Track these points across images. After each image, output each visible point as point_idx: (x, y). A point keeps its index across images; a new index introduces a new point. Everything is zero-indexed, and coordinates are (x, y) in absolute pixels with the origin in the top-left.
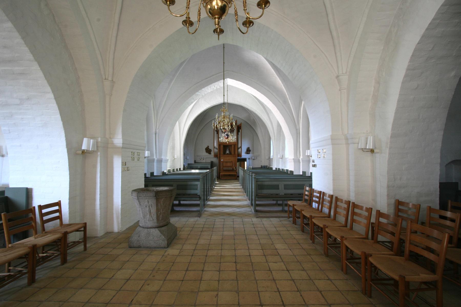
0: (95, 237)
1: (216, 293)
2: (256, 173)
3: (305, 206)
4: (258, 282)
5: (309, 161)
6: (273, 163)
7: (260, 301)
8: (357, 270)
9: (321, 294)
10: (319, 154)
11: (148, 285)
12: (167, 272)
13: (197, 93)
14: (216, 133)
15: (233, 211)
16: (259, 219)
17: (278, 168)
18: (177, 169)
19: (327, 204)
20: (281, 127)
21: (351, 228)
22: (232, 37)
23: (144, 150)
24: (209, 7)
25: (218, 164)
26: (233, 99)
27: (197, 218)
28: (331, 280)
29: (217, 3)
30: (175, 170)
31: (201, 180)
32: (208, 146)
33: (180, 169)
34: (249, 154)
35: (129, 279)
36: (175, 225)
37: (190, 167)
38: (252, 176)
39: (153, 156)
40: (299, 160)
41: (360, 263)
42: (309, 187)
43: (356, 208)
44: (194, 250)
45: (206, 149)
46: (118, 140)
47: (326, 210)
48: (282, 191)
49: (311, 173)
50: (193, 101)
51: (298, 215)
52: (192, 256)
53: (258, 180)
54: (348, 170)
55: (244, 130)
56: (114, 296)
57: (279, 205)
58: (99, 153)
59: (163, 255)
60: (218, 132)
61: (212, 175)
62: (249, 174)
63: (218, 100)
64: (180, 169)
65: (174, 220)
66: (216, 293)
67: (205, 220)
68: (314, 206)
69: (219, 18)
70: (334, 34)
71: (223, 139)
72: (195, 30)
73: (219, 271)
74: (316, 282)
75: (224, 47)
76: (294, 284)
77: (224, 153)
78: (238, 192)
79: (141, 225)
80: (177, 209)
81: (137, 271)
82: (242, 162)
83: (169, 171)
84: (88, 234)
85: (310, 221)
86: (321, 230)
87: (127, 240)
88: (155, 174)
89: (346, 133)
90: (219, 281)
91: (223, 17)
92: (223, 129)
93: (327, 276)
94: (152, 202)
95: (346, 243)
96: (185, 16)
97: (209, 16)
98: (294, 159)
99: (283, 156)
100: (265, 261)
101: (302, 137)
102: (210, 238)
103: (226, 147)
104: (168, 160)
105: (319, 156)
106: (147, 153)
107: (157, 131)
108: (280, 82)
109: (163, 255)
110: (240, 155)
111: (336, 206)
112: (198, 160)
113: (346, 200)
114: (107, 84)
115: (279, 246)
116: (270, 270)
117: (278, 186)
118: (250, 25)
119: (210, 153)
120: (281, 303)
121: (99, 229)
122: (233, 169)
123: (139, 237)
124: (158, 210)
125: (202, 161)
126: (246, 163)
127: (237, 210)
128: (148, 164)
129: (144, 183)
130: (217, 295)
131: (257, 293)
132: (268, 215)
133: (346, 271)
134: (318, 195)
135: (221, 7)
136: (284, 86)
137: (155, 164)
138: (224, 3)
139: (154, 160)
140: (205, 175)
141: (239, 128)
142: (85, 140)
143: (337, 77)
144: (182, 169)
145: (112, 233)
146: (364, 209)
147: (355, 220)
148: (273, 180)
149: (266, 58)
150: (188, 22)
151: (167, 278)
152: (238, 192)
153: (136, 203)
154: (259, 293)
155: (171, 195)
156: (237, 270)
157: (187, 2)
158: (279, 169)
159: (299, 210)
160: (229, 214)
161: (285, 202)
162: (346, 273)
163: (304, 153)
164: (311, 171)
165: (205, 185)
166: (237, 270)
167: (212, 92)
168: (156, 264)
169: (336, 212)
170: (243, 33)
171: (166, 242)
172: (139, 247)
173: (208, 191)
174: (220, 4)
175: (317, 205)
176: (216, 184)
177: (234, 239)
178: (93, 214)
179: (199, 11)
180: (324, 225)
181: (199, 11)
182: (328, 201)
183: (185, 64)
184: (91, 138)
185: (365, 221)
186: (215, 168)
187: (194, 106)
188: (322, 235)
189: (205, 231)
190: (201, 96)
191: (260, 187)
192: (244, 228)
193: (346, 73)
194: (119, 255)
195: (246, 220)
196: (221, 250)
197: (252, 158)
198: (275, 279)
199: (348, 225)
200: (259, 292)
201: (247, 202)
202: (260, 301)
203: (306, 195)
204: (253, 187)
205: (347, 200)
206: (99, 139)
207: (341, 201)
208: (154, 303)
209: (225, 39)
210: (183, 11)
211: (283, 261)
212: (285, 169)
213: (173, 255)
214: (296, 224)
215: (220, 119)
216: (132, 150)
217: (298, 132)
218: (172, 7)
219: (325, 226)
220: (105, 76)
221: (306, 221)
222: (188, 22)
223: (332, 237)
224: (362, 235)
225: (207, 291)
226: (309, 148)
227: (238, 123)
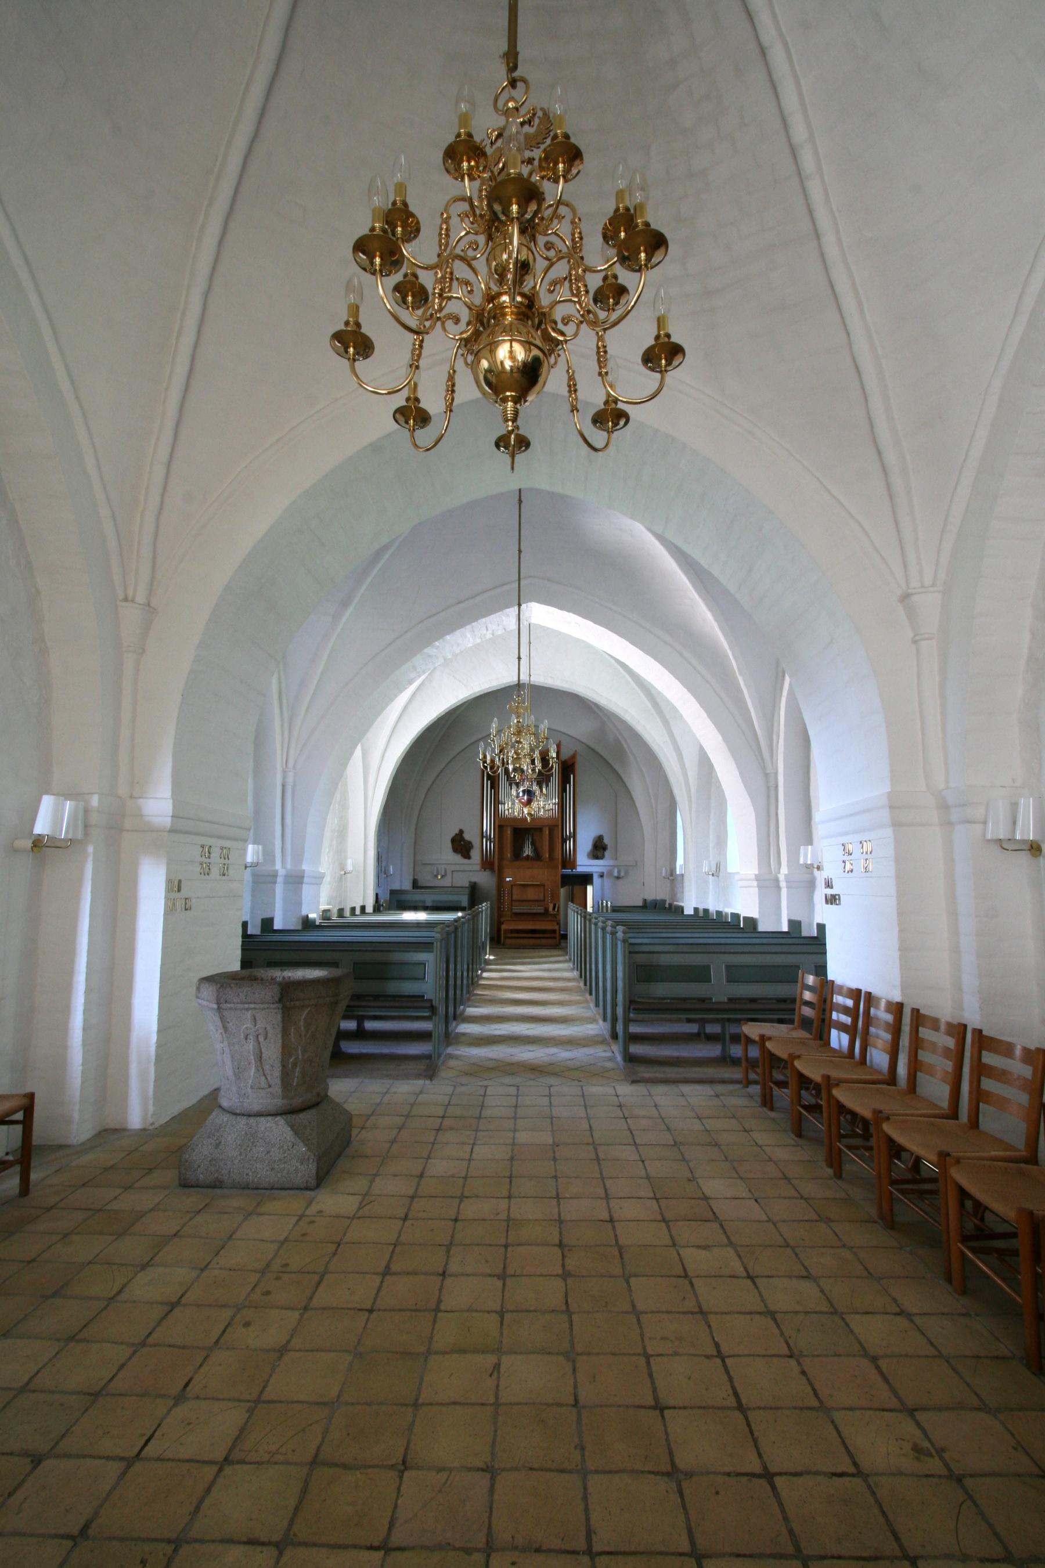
0: (61, 1147)
1: (491, 1359)
2: (630, 926)
3: (802, 1042)
4: (644, 1318)
5: (811, 885)
6: (686, 889)
7: (655, 1391)
8: (1004, 1279)
9: (878, 1367)
10: (846, 858)
11: (247, 1324)
12: (316, 1277)
13: (428, 650)
14: (487, 784)
15: (546, 1059)
16: (641, 1089)
17: (701, 907)
18: (353, 909)
19: (881, 1036)
20: (711, 766)
21: (974, 1123)
22: (557, 463)
23: (245, 841)
24: (485, 364)
25: (494, 892)
26: (545, 673)
27: (421, 1082)
28: (909, 1316)
29: (511, 352)
30: (347, 913)
31: (437, 946)
32: (461, 832)
33: (363, 908)
34: (602, 857)
35: (178, 1303)
36: (345, 1106)
37: (399, 901)
38: (613, 934)
39: (274, 863)
40: (777, 880)
41: (1015, 1253)
42: (817, 975)
43: (990, 1050)
44: (413, 1197)
45: (453, 840)
46: (159, 805)
47: (879, 1058)
48: (719, 989)
49: (821, 927)
50: (413, 675)
51: (778, 1076)
52: (405, 1218)
53: (637, 949)
54: (953, 914)
55: (583, 775)
56: (122, 1366)
57: (711, 1038)
58: (90, 849)
59: (301, 1217)
60: (494, 781)
61: (475, 932)
62: (603, 929)
63: (499, 674)
64: (363, 908)
65: (341, 1088)
66: (491, 1359)
67: (449, 1090)
68: (834, 1043)
69: (517, 401)
70: (891, 457)
71: (513, 806)
72: (434, 438)
73: (503, 1277)
74: (856, 1322)
75: (520, 501)
76: (776, 1331)
77: (517, 854)
78: (562, 990)
79: (225, 1103)
80: (351, 1048)
81: (205, 1273)
82: (577, 889)
83: (326, 915)
84: (36, 1139)
85: (824, 1095)
86: (860, 1130)
87: (174, 1159)
88: (277, 925)
89: (942, 786)
90: (501, 1314)
91: (530, 398)
92: (515, 770)
93: (895, 1300)
94: (270, 1019)
95: (959, 1176)
96: (405, 393)
97: (484, 393)
98: (758, 878)
99: (718, 867)
100: (667, 1241)
101: (787, 804)
102: (467, 1156)
103: (522, 837)
104: (322, 877)
105: (848, 867)
106: (252, 853)
107: (290, 779)
108: (709, 616)
109: (301, 1217)
110: (569, 861)
111: (917, 1043)
112: (425, 879)
113: (949, 1020)
114: (131, 616)
115: (716, 1186)
116: (686, 1276)
117: (707, 968)
118: (615, 424)
119: (467, 856)
120: (731, 1401)
121: (76, 1115)
122: (546, 910)
123: (217, 1146)
124: (286, 1050)
125: (440, 882)
126: (590, 889)
127: (563, 1054)
128: (254, 891)
129: (238, 953)
130: (497, 1366)
131: (643, 1360)
132: (672, 1072)
133: (962, 1282)
134: (850, 1003)
135: (525, 364)
136: (721, 628)
137: (279, 889)
138: (535, 352)
139: (275, 876)
140: (451, 929)
141: (568, 768)
142: (47, 802)
143: (905, 597)
144: (369, 909)
145: (120, 1131)
146: (1018, 1052)
147: (988, 1093)
148: (685, 949)
149: (660, 538)
150: (412, 415)
151: (315, 1302)
152: (562, 990)
153: (212, 1024)
154: (648, 1363)
155: (334, 997)
156: (565, 1275)
157: (414, 349)
158: (706, 911)
159: (784, 1055)
160: (536, 1070)
161: (733, 1029)
162: (964, 1291)
163: (794, 856)
164: (818, 919)
165: (452, 966)
166: (565, 1275)
167: (477, 647)
168: (275, 1246)
169: (915, 1066)
170: (595, 450)
171: (313, 1167)
172: (216, 1184)
173: (460, 987)
174: (520, 354)
175: (845, 1038)
176: (488, 962)
177: (555, 1159)
178: (61, 1063)
179: (451, 378)
180: (877, 1113)
181: (451, 378)
182: (887, 1023)
183: (387, 556)
184: (68, 796)
185: (1024, 1098)
186: (484, 906)
187: (418, 688)
188: (870, 1149)
189: (451, 1129)
190: (441, 660)
191: (643, 972)
192: (588, 1118)
193: (933, 585)
194: (144, 1214)
195: (597, 1089)
196: (510, 1197)
197: (610, 873)
198: (705, 1308)
199: (964, 1114)
200: (648, 1357)
201: (598, 1028)
202: (655, 1391)
203: (807, 1003)
204: (620, 975)
205: (955, 1022)
206: (95, 801)
207: (934, 1024)
208: (264, 1397)
209: (534, 472)
210: (400, 376)
211: (730, 1243)
212: (729, 910)
213: (337, 1217)
214: (772, 1109)
215: (504, 737)
216: (203, 840)
217: (772, 784)
218: (361, 365)
219: (880, 1116)
220: (125, 589)
221: (808, 1098)
222: (412, 415)
223: (904, 1155)
224: (1009, 1147)
225: (459, 1350)
226: (809, 841)
227: (566, 754)
